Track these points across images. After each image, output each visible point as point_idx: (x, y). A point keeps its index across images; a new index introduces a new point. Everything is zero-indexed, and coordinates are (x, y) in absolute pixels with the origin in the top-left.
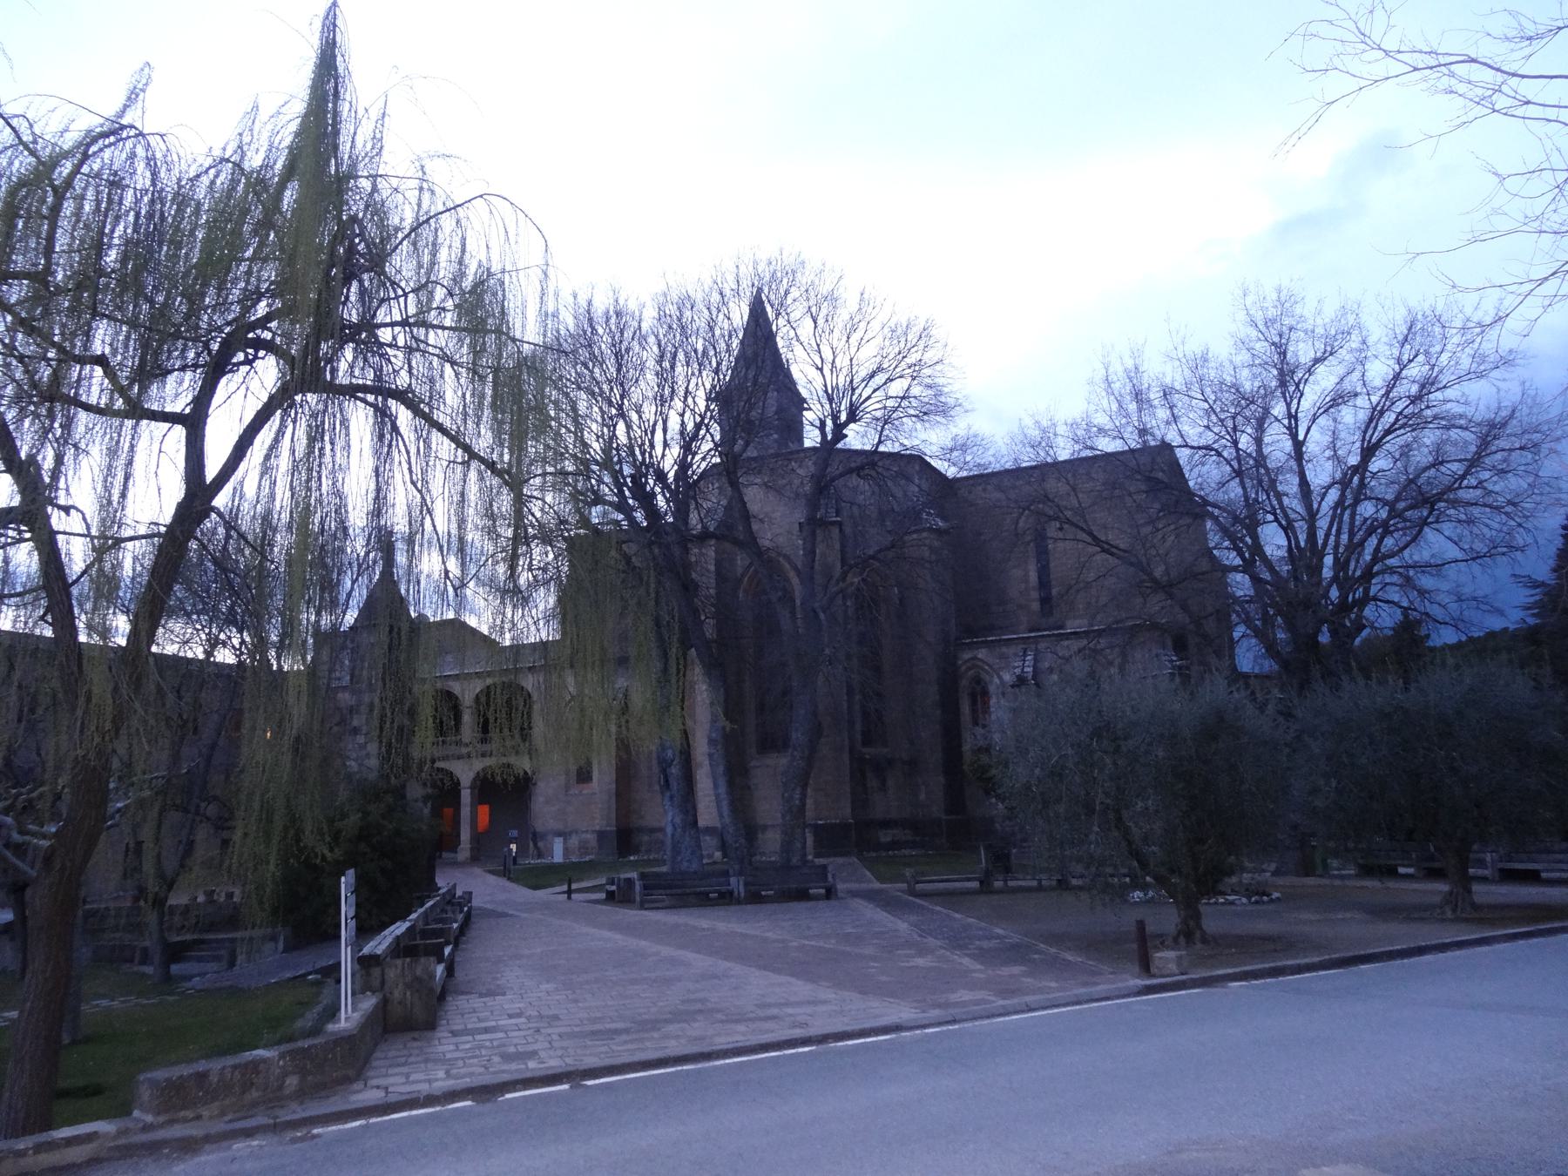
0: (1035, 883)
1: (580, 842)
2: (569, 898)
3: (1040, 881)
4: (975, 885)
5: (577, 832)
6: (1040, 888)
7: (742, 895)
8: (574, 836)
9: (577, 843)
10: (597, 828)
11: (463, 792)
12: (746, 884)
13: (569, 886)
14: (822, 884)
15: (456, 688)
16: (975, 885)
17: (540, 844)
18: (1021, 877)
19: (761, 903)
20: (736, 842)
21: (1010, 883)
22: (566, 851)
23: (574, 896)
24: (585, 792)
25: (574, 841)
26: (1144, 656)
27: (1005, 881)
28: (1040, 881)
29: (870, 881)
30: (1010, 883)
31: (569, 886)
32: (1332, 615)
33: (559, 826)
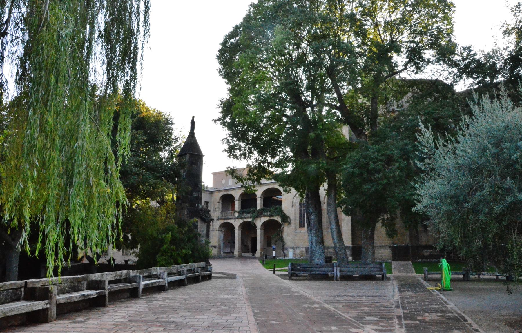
0: (495, 277)
1: (300, 251)
2: (274, 273)
3: (497, 276)
4: (461, 276)
5: (299, 247)
6: (497, 280)
7: (339, 276)
8: (298, 249)
9: (299, 251)
10: (306, 246)
11: (258, 230)
12: (341, 271)
13: (274, 269)
14: (380, 273)
15: (232, 193)
16: (461, 276)
17: (285, 252)
18: (486, 273)
19: (352, 280)
20: (340, 251)
21: (481, 276)
22: (294, 254)
23: (276, 272)
24: (302, 231)
25: (298, 251)
26: (34, 142)
27: (479, 275)
28: (497, 276)
29: (412, 272)
30: (481, 276)
31: (274, 269)
32: (286, 80)
33: (292, 245)
